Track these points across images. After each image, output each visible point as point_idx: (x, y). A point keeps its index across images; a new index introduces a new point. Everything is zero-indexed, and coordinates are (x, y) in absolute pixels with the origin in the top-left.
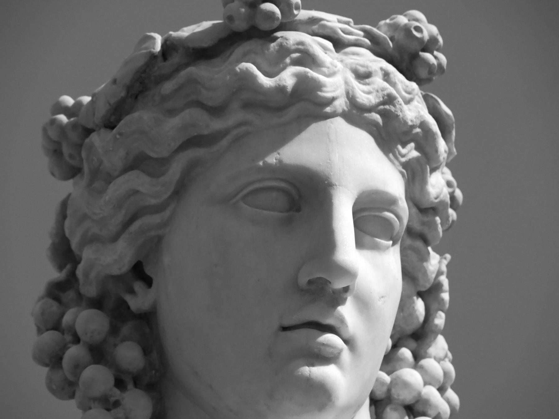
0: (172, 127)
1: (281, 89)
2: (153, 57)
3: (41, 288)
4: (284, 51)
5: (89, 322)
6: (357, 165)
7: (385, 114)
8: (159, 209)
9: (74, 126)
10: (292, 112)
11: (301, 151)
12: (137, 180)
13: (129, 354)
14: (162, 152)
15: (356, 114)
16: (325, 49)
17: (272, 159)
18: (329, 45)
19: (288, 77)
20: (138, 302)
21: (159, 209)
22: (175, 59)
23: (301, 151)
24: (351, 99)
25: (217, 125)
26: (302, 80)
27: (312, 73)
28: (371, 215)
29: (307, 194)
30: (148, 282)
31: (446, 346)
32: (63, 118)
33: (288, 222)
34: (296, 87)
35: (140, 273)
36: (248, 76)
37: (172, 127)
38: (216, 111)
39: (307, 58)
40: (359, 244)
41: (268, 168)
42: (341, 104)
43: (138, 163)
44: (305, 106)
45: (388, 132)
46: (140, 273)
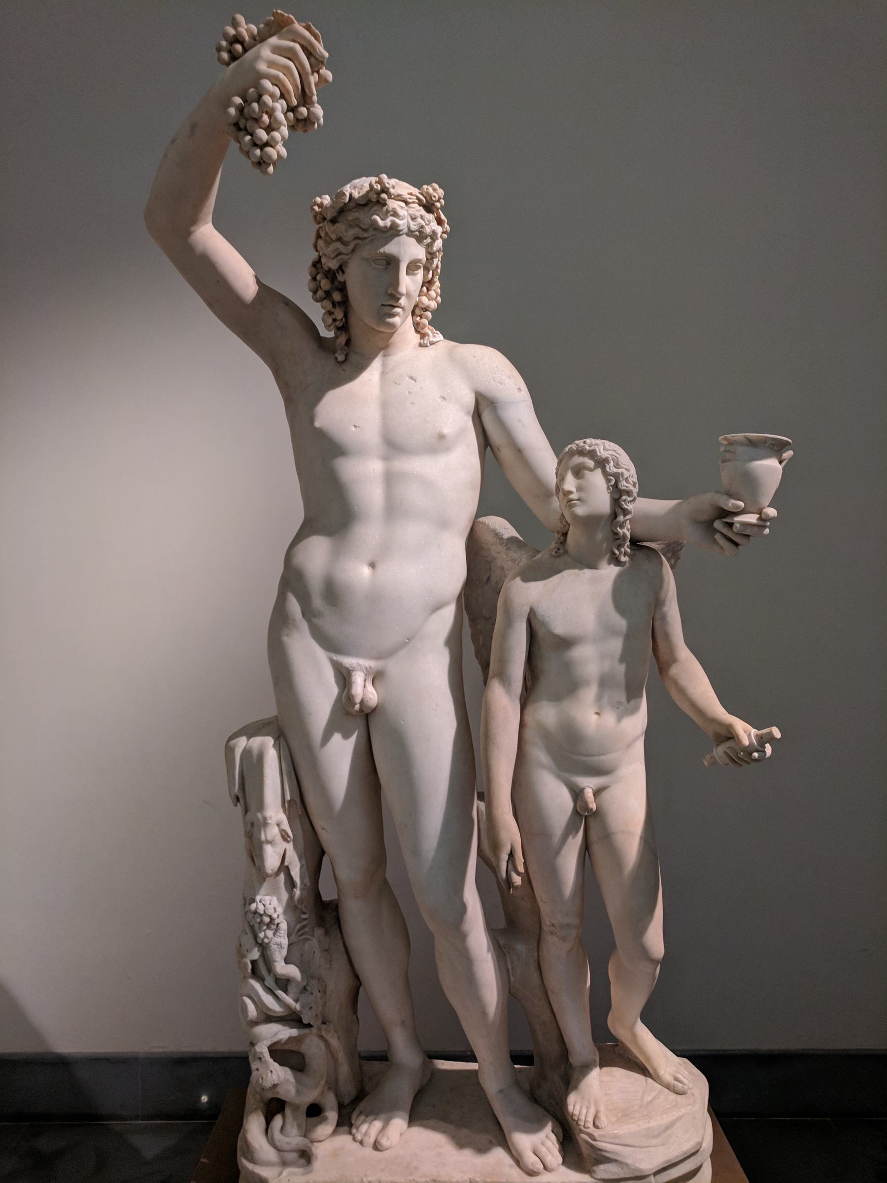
0: (352, 232)
1: (386, 227)
2: (345, 204)
3: (310, 263)
4: (388, 211)
5: (325, 284)
6: (410, 250)
7: (420, 232)
8: (347, 255)
9: (321, 213)
10: (390, 233)
11: (390, 248)
12: (338, 245)
13: (337, 296)
14: (348, 240)
15: (410, 233)
16: (402, 208)
17: (382, 250)
18: (403, 204)
19: (388, 222)
20: (340, 278)
21: (347, 255)
22: (352, 204)
23: (390, 248)
24: (409, 228)
25: (365, 235)
26: (393, 223)
27: (397, 221)
28: (412, 267)
29: (392, 263)
30: (343, 272)
31: (441, 245)
32: (316, 208)
33: (386, 269)
34: (391, 226)
35: (341, 269)
36: (375, 222)
37: (352, 232)
38: (364, 230)
39: (395, 214)
40: (407, 274)
41: (381, 254)
42: (405, 230)
43: (339, 239)
44: (393, 232)
45: (420, 236)
46: (341, 269)
